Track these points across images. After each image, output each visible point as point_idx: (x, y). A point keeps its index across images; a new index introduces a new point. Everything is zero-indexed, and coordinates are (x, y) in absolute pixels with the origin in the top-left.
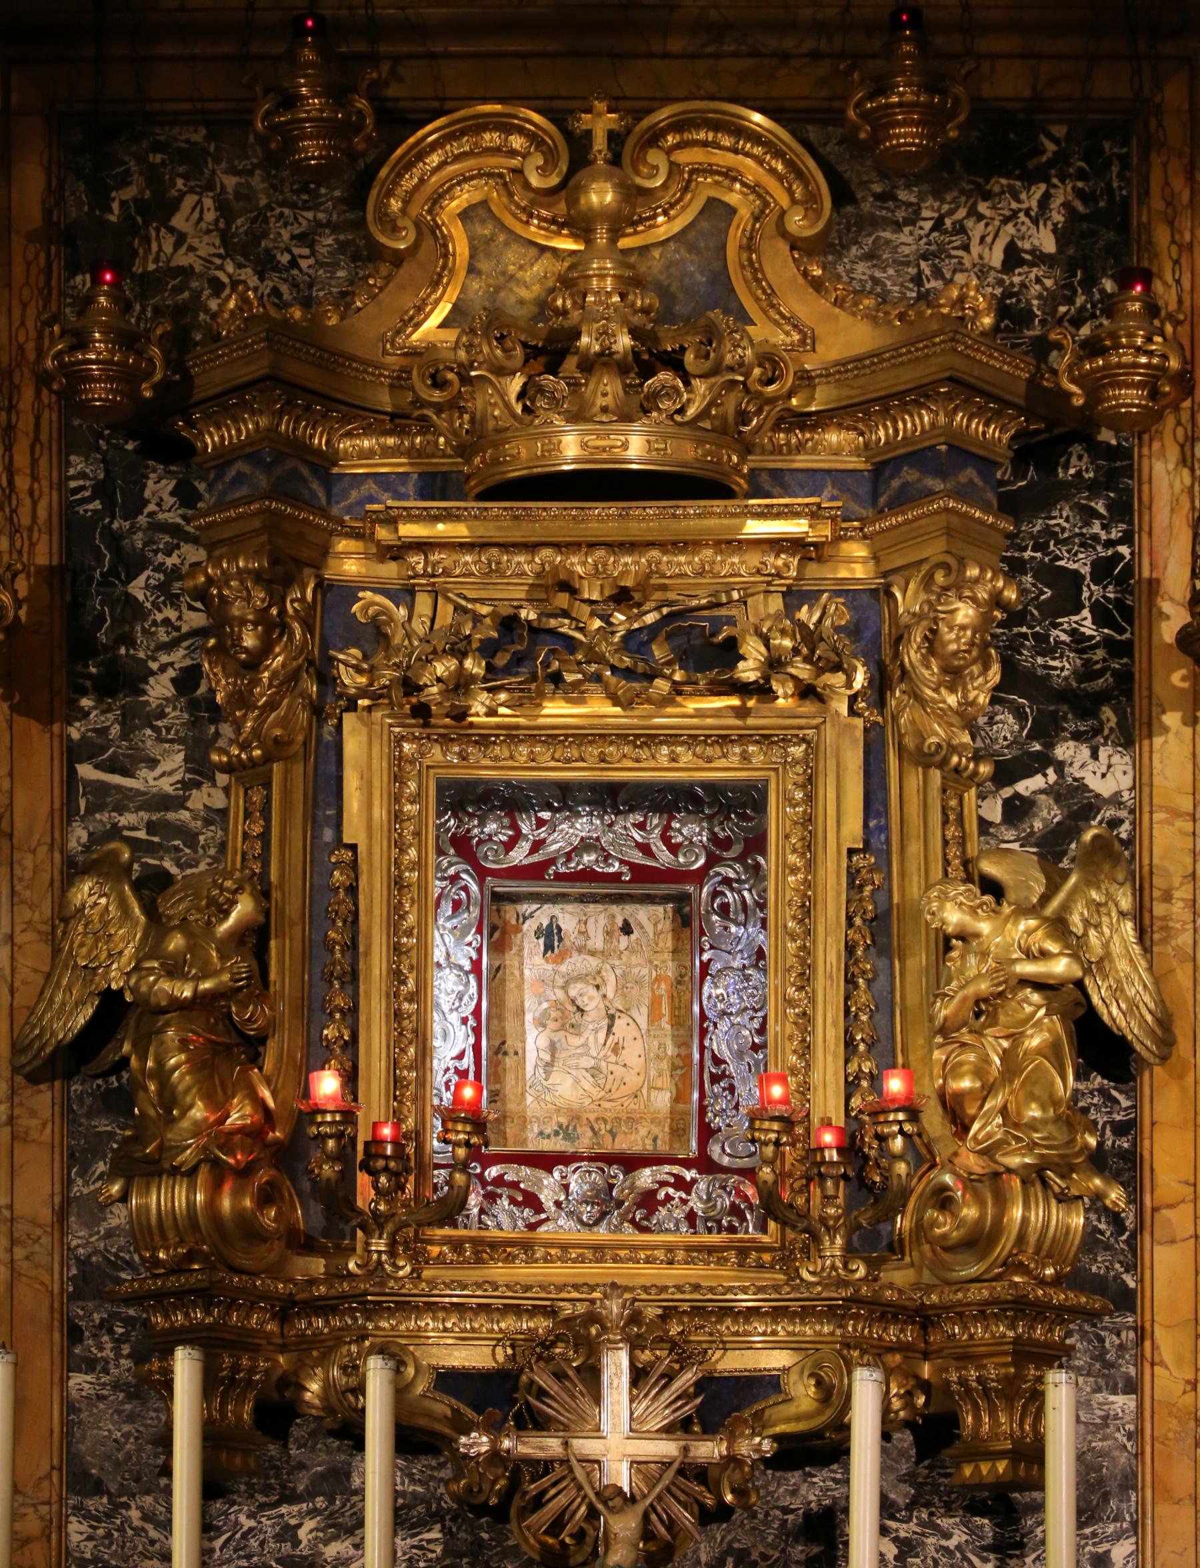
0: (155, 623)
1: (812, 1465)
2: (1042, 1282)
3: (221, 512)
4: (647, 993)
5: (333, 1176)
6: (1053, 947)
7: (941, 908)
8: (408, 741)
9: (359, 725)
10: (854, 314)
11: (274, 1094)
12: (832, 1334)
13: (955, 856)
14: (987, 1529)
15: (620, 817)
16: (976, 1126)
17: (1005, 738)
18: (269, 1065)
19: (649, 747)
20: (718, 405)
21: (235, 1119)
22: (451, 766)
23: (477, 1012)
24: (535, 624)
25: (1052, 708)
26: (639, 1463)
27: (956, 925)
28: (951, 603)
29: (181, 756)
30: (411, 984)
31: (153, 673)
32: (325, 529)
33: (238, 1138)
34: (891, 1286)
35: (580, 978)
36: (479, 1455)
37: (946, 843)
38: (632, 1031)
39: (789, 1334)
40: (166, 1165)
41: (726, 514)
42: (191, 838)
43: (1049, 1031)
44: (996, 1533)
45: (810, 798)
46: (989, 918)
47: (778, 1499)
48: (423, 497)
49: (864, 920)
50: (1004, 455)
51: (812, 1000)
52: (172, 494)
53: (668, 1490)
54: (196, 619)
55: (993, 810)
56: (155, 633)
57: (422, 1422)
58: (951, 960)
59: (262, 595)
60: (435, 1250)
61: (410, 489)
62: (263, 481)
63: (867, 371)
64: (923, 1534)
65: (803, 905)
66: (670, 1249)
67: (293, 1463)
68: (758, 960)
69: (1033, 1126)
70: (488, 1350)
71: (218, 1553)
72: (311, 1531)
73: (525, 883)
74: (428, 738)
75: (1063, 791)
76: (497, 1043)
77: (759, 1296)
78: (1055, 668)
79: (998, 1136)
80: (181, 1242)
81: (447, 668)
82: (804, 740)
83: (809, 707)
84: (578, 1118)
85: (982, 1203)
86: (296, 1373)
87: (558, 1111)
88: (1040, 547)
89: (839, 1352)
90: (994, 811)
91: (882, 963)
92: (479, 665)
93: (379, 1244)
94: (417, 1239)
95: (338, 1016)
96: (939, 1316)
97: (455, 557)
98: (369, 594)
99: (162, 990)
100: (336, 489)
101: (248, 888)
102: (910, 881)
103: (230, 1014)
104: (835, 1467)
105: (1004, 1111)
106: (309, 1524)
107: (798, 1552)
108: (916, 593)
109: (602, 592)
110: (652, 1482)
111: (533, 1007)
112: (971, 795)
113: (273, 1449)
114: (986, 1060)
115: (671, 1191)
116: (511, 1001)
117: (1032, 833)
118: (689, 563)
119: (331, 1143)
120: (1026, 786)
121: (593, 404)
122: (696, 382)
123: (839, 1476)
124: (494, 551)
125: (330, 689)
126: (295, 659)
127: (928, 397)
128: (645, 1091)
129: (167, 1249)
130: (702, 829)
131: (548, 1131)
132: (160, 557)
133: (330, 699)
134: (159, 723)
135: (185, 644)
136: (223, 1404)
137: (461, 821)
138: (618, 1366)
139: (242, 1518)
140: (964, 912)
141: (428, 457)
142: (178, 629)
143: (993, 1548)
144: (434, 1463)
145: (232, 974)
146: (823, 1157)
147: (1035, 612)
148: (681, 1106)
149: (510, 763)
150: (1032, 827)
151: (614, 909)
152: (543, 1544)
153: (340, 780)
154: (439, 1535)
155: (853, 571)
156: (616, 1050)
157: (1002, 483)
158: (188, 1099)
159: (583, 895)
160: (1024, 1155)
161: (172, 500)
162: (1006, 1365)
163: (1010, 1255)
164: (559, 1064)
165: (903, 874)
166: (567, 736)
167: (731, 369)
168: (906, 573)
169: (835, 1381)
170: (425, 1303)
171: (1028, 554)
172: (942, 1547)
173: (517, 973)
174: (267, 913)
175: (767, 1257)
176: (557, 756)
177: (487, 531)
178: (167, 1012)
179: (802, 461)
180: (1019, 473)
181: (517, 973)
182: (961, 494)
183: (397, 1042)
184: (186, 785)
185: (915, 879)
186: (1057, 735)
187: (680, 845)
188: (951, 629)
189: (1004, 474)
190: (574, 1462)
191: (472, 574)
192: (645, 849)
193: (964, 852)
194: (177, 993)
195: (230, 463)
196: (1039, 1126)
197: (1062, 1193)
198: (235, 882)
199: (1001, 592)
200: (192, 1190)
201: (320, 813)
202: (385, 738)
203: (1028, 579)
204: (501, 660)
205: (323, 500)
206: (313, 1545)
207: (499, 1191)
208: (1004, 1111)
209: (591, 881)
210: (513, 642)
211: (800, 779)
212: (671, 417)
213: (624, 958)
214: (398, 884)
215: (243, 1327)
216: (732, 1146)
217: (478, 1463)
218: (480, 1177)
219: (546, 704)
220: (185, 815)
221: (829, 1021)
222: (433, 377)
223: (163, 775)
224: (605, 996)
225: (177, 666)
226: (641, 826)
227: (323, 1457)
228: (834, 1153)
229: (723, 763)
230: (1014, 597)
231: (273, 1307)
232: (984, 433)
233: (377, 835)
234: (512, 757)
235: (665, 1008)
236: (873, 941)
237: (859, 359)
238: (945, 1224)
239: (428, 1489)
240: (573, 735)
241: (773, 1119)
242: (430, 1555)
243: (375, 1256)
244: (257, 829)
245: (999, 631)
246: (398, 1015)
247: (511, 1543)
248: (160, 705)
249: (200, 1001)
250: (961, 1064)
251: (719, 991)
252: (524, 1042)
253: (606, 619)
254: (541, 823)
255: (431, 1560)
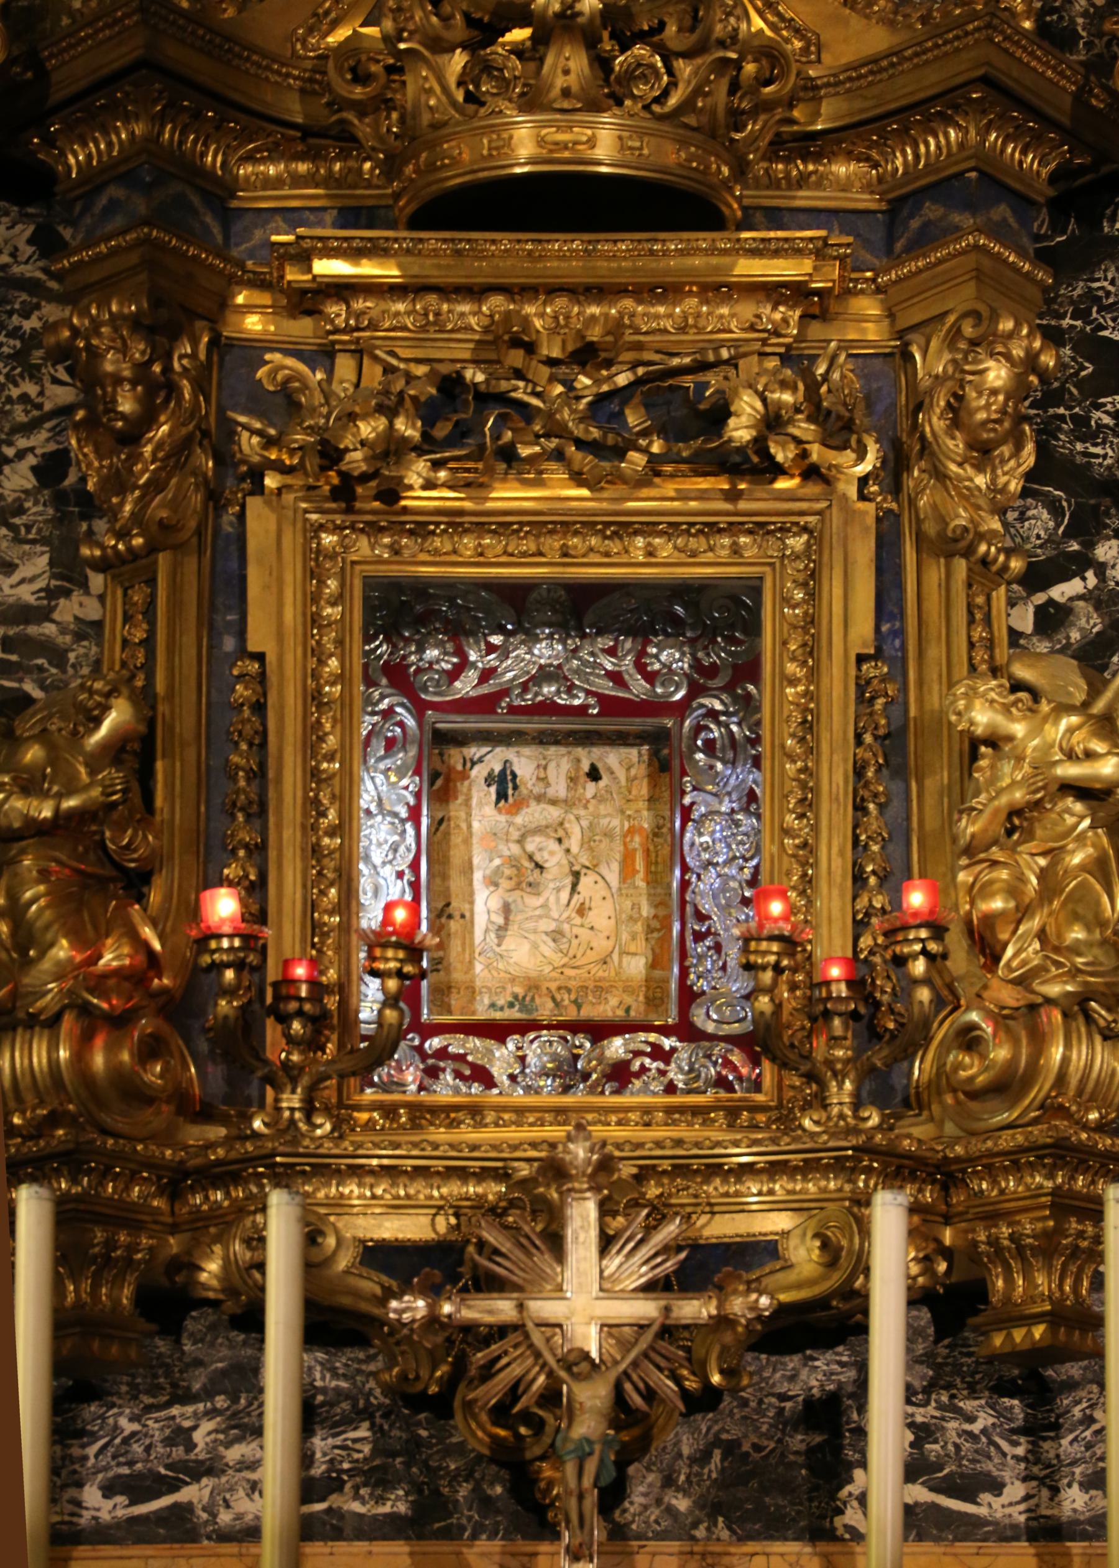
0: (9, 400)
1: (814, 1347)
2: (1085, 1127)
3: (88, 248)
4: (618, 847)
5: (231, 1013)
6: (1099, 747)
7: (969, 707)
8: (327, 531)
9: (266, 511)
10: (867, 17)
11: (161, 937)
12: (840, 1190)
13: (983, 661)
14: (1017, 1410)
15: (587, 641)
16: (1009, 952)
17: (1038, 537)
18: (155, 897)
19: (621, 538)
20: (706, 95)
21: (109, 959)
22: (380, 561)
23: (415, 866)
24: (483, 388)
25: (1092, 502)
26: (610, 1326)
27: (987, 726)
28: (981, 362)
29: (45, 559)
30: (332, 814)
31: (8, 461)
32: (221, 272)
33: (112, 982)
34: (909, 1136)
35: (539, 830)
36: (414, 1321)
37: (971, 645)
38: (601, 890)
39: (789, 1192)
40: (21, 1015)
41: (712, 251)
42: (58, 656)
43: (1094, 845)
44: (1027, 1414)
45: (812, 596)
46: (1024, 718)
47: (774, 1385)
48: (343, 227)
49: (876, 737)
50: (1043, 191)
51: (815, 829)
52: (30, 242)
53: (645, 1355)
54: (64, 395)
55: (1023, 618)
56: (9, 413)
57: (346, 1301)
58: (980, 770)
59: (142, 346)
60: (364, 1116)
61: (329, 217)
62: (141, 206)
63: (885, 75)
64: (943, 1419)
65: (805, 721)
66: (647, 1110)
67: (187, 1360)
68: (749, 803)
69: (1076, 949)
70: (425, 1221)
71: (92, 1460)
72: (209, 1433)
73: (472, 718)
74: (352, 527)
75: (1104, 597)
76: (440, 905)
77: (755, 1149)
78: (1097, 456)
79: (1036, 962)
80: (42, 1103)
81: (374, 429)
82: (805, 529)
83: (814, 489)
84: (537, 987)
85: (1016, 1042)
86: (189, 1252)
87: (513, 980)
88: (1081, 314)
89: (849, 1209)
90: (1024, 619)
91: (897, 786)
92: (414, 427)
93: (292, 1100)
94: (341, 1104)
95: (242, 853)
96: (964, 1171)
97: (383, 306)
98: (277, 357)
99: (12, 808)
100: (237, 227)
101: (125, 691)
102: (930, 693)
103: (103, 841)
104: (840, 1349)
105: (1042, 935)
106: (207, 1426)
107: (798, 1441)
108: (940, 352)
109: (564, 348)
110: (625, 1346)
111: (482, 864)
112: (1000, 595)
113: (162, 1346)
114: (1022, 879)
115: (647, 1061)
116: (456, 856)
117: (1068, 645)
118: (670, 316)
119: (229, 974)
120: (1061, 592)
121: (551, 86)
122: (680, 64)
123: (845, 1359)
124: (432, 299)
125: (231, 472)
126: (184, 425)
127: (956, 107)
128: (615, 956)
129: (23, 1113)
130: (683, 654)
131: (501, 1002)
132: (16, 320)
133: (230, 482)
134: (17, 521)
135: (48, 425)
136: (96, 1287)
137: (395, 646)
138: (584, 1218)
139: (123, 1422)
140: (996, 711)
141: (350, 187)
142: (39, 406)
143: (1024, 1431)
144: (361, 1355)
145: (105, 787)
146: (829, 992)
147: (1074, 391)
148: (658, 973)
149: (454, 558)
150: (1068, 638)
151: (580, 752)
152: (494, 1438)
153: (243, 579)
154: (367, 1434)
155: (864, 331)
156: (581, 911)
157: (1037, 238)
158: (49, 936)
159: (542, 732)
160: (1066, 983)
161: (30, 250)
162: (1044, 1218)
163: (1048, 1096)
164: (513, 928)
165: (920, 683)
166: (522, 524)
167: (722, 44)
168: (928, 330)
169: (844, 1243)
170: (349, 1166)
171: (1067, 322)
172: (965, 1432)
173: (464, 826)
174: (151, 723)
175: (761, 1118)
176: (510, 550)
177: (427, 269)
178: (22, 838)
179: (804, 198)
180: (1058, 227)
181: (464, 826)
182: (996, 231)
183: (315, 882)
184: (52, 594)
185: (936, 687)
186: (1098, 533)
187: (656, 673)
188: (980, 394)
189: (1040, 226)
190: (530, 1325)
191: (404, 328)
192: (616, 678)
193: (992, 657)
194: (33, 813)
195: (99, 189)
196: (1083, 949)
197: (1108, 1027)
198: (107, 683)
199: (1037, 355)
200: (53, 1047)
201: (218, 618)
202: (299, 525)
203: (1067, 351)
204: (442, 430)
205: (219, 239)
206: (211, 1448)
207: (442, 1064)
208: (1042, 935)
209: (552, 714)
210: (456, 411)
211: (801, 577)
212: (646, 108)
213: (591, 807)
214: (315, 698)
215: (121, 1200)
216: (718, 1010)
217: (412, 1330)
218: (420, 1050)
219: (497, 485)
220: (49, 629)
221: (835, 850)
222: (353, 70)
223: (22, 581)
224: (568, 851)
225: (38, 451)
226: (611, 652)
227: (225, 1352)
228: (843, 987)
229: (709, 557)
230: (1051, 364)
231: (160, 1178)
232: (1021, 162)
233: (290, 642)
234: (455, 552)
235: (640, 864)
236: (886, 760)
237: (874, 60)
238: (972, 1066)
239: (354, 1384)
240: (529, 523)
241: (771, 938)
242: (356, 1456)
243: (287, 1114)
244: (139, 635)
245: (1033, 412)
246: (316, 850)
247: (454, 1440)
248: (19, 499)
249: (62, 823)
250: (991, 882)
251: (704, 839)
252: (472, 903)
253: (569, 385)
254: (491, 648)
255: (357, 1461)
